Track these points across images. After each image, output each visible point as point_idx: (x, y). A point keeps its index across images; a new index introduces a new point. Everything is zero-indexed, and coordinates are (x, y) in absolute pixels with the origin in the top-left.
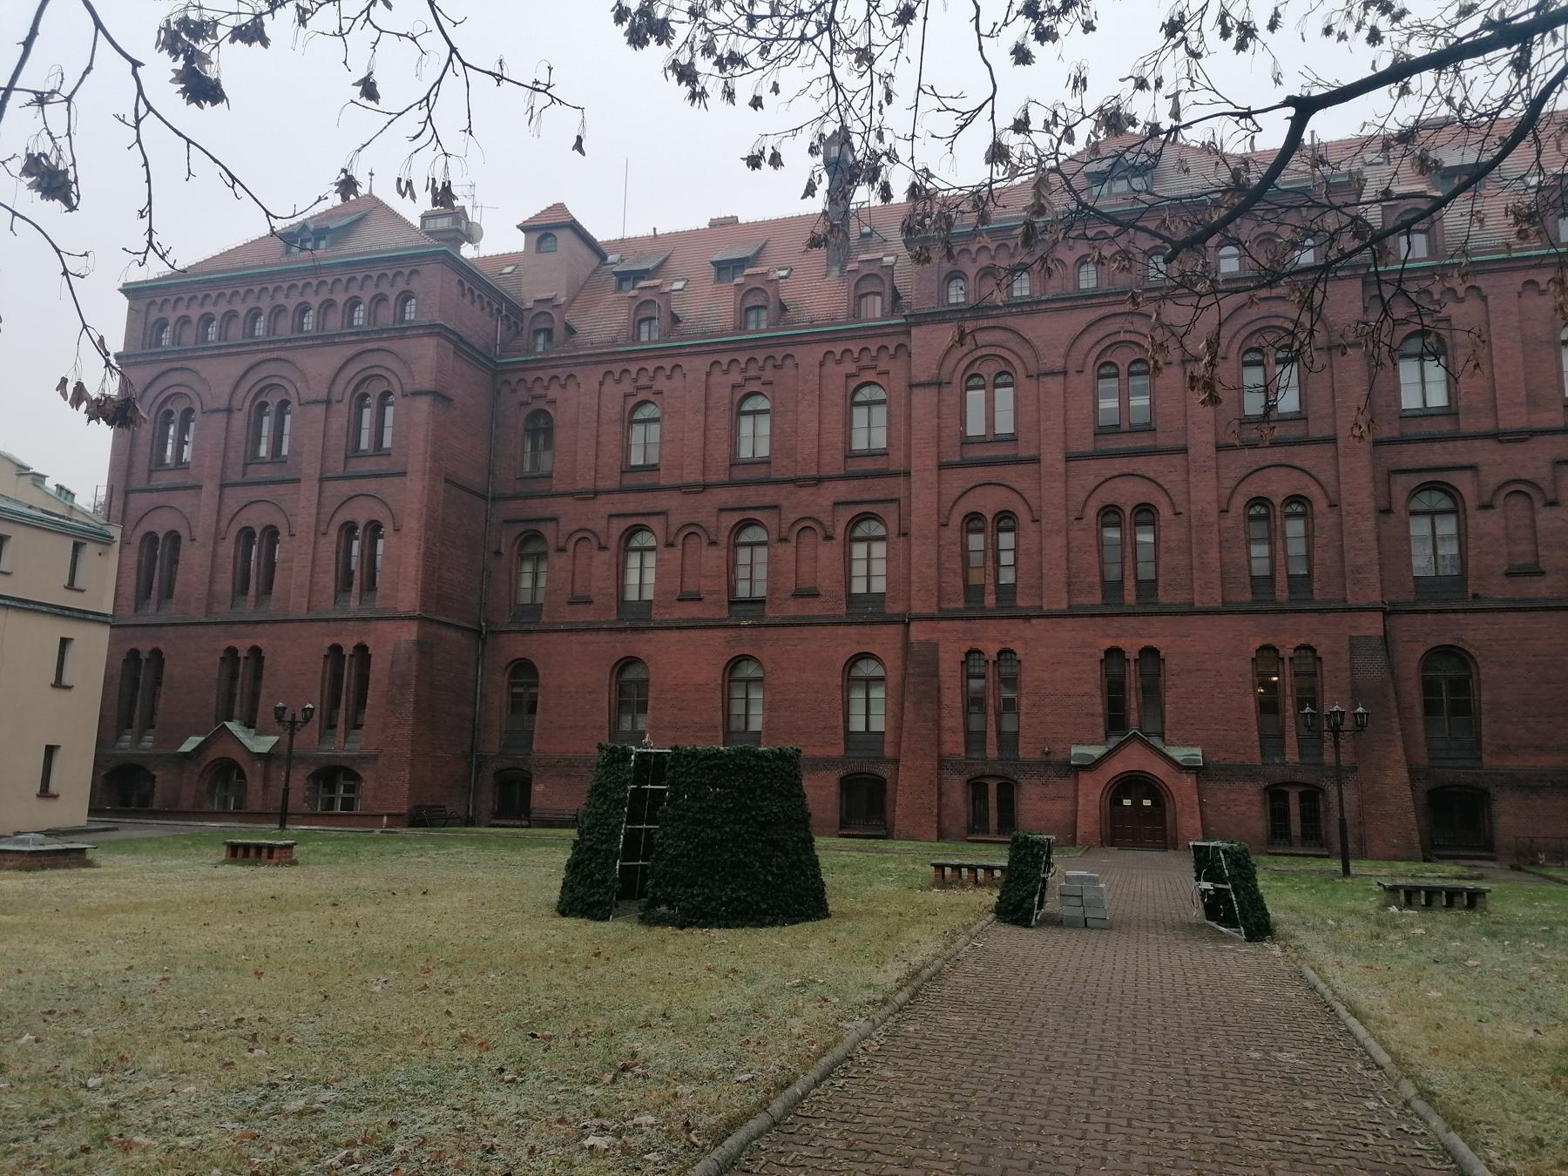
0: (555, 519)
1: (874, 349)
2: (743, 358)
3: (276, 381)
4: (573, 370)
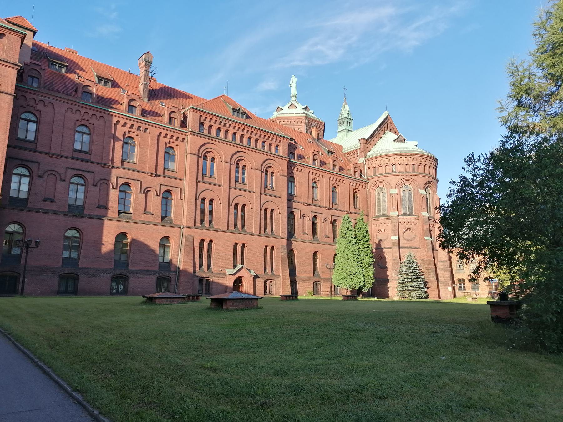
0: (38, 163)
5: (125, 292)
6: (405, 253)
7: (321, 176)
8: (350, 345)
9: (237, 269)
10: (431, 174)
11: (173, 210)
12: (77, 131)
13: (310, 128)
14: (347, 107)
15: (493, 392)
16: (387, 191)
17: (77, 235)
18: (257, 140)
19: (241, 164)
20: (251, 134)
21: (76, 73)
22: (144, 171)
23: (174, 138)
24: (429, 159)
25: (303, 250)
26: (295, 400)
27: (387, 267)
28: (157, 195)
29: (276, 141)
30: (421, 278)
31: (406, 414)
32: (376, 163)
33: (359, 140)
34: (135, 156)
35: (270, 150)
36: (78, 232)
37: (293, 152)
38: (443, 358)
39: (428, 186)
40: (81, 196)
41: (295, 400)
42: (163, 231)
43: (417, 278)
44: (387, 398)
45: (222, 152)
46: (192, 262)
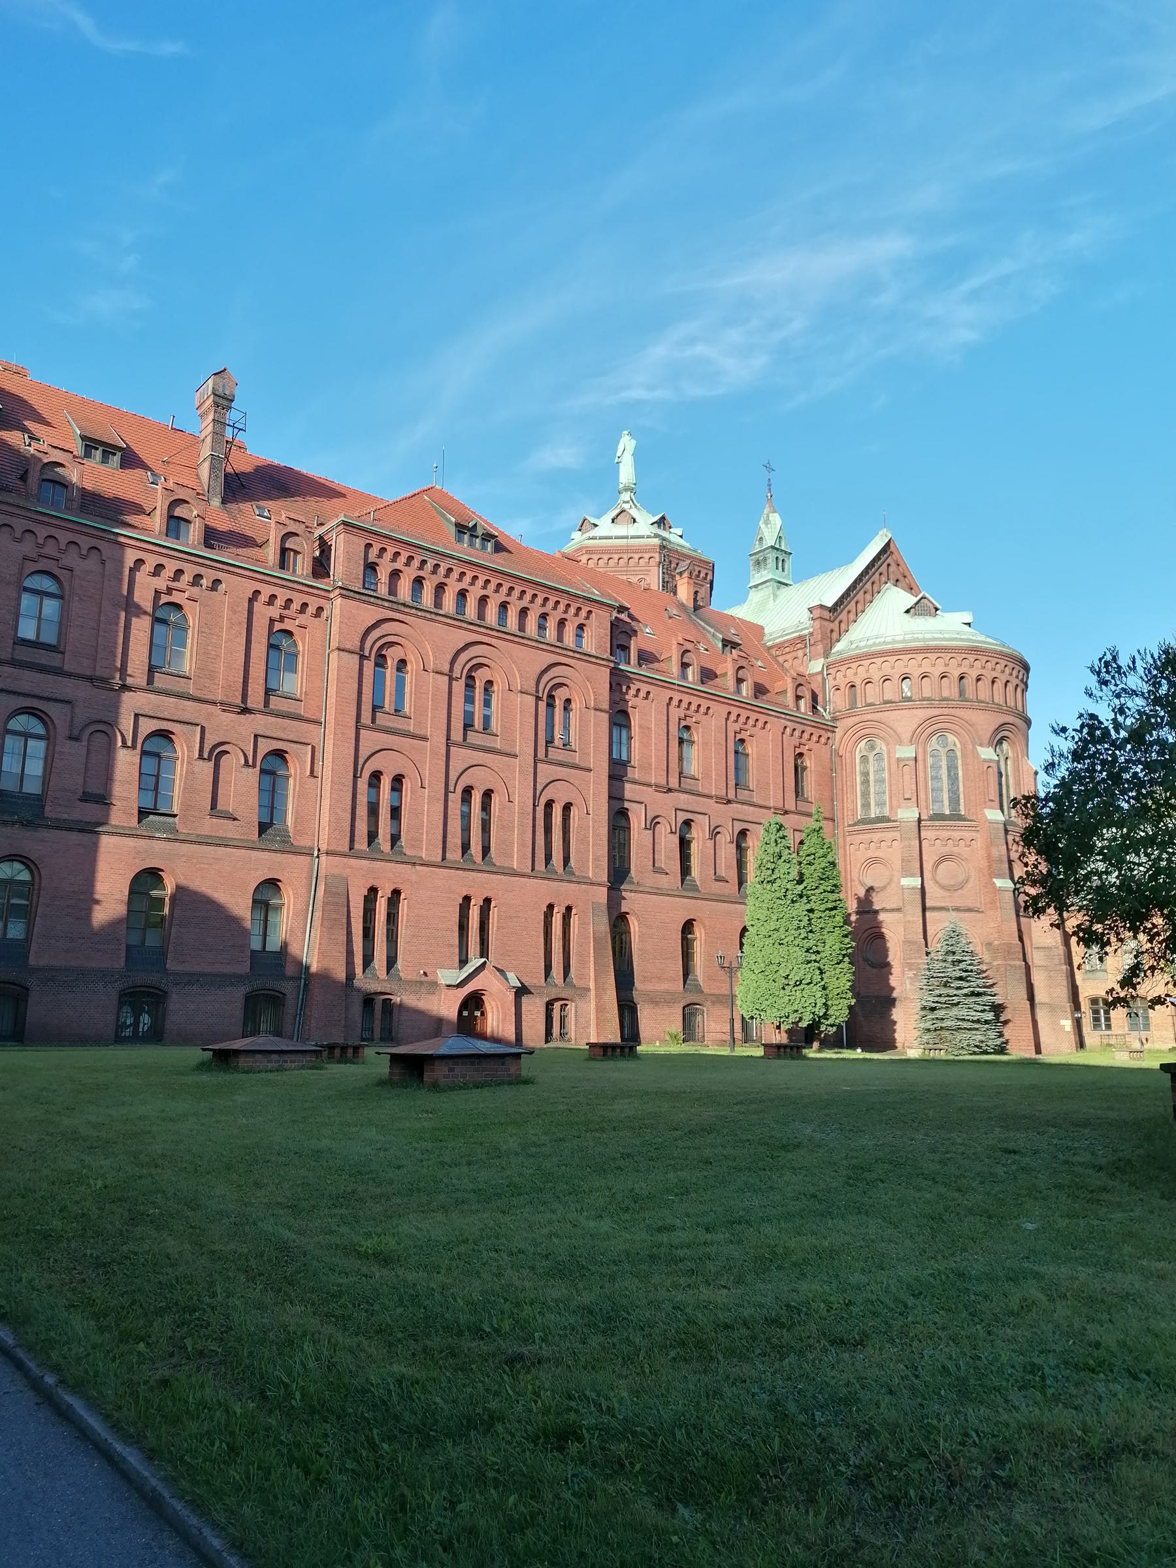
5: (156, 1036)
6: (939, 924)
7: (702, 710)
8: (772, 1188)
9: (469, 969)
10: (1011, 703)
11: (290, 807)
12: (26, 589)
13: (673, 577)
14: (776, 520)
15: (1163, 1325)
16: (889, 752)
17: (25, 876)
18: (524, 612)
19: (481, 676)
20: (509, 595)
21: (24, 430)
22: (210, 697)
23: (295, 606)
24: (1003, 663)
25: (652, 917)
26: (604, 1348)
27: (888, 965)
28: (246, 764)
29: (576, 615)
30: (984, 994)
31: (912, 1388)
32: (857, 674)
33: (810, 610)
34: (188, 654)
35: (560, 638)
36: (28, 867)
37: (623, 644)
38: (1030, 1226)
39: (1003, 738)
40: (35, 768)
41: (604, 1348)
42: (264, 864)
43: (973, 994)
44: (861, 1343)
45: (428, 644)
46: (343, 949)
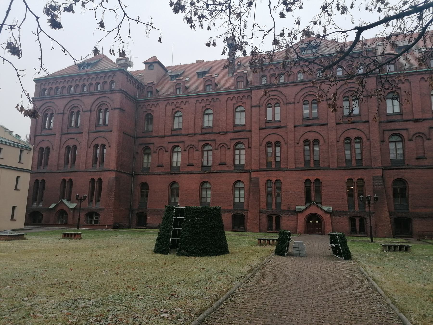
0: (153, 144)
1: (241, 96)
2: (205, 99)
3: (76, 105)
4: (158, 102)
